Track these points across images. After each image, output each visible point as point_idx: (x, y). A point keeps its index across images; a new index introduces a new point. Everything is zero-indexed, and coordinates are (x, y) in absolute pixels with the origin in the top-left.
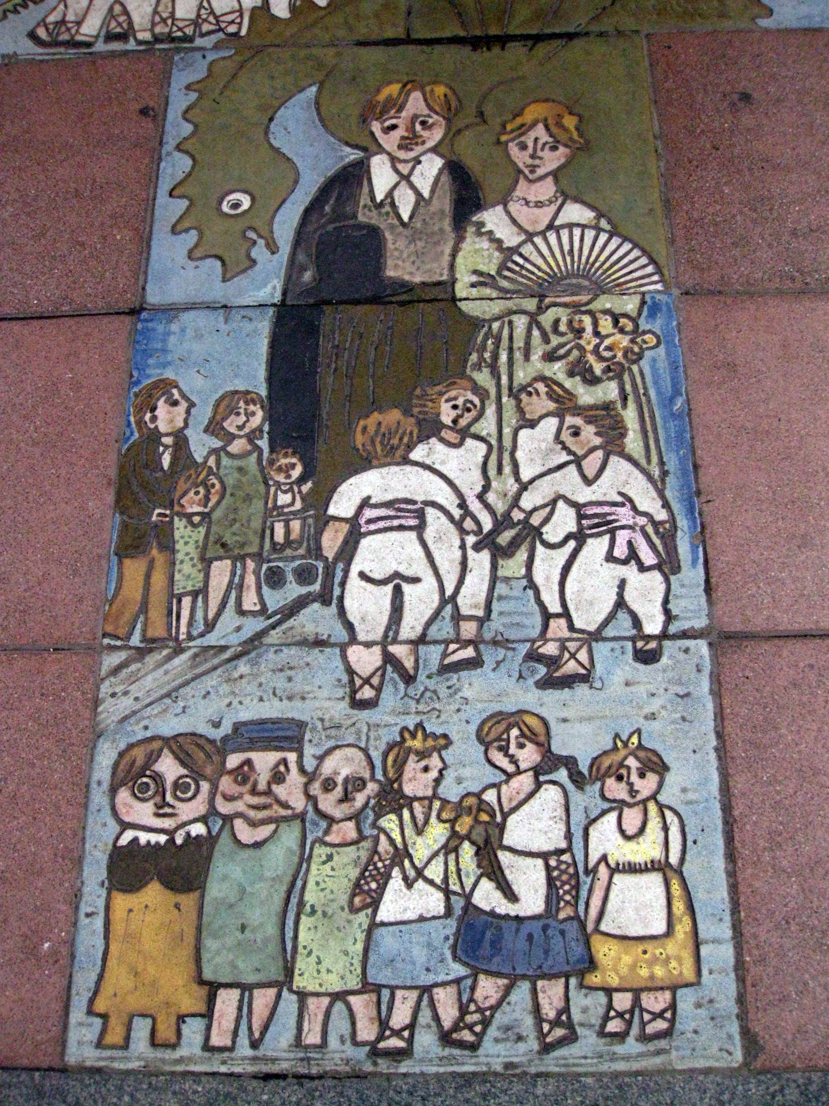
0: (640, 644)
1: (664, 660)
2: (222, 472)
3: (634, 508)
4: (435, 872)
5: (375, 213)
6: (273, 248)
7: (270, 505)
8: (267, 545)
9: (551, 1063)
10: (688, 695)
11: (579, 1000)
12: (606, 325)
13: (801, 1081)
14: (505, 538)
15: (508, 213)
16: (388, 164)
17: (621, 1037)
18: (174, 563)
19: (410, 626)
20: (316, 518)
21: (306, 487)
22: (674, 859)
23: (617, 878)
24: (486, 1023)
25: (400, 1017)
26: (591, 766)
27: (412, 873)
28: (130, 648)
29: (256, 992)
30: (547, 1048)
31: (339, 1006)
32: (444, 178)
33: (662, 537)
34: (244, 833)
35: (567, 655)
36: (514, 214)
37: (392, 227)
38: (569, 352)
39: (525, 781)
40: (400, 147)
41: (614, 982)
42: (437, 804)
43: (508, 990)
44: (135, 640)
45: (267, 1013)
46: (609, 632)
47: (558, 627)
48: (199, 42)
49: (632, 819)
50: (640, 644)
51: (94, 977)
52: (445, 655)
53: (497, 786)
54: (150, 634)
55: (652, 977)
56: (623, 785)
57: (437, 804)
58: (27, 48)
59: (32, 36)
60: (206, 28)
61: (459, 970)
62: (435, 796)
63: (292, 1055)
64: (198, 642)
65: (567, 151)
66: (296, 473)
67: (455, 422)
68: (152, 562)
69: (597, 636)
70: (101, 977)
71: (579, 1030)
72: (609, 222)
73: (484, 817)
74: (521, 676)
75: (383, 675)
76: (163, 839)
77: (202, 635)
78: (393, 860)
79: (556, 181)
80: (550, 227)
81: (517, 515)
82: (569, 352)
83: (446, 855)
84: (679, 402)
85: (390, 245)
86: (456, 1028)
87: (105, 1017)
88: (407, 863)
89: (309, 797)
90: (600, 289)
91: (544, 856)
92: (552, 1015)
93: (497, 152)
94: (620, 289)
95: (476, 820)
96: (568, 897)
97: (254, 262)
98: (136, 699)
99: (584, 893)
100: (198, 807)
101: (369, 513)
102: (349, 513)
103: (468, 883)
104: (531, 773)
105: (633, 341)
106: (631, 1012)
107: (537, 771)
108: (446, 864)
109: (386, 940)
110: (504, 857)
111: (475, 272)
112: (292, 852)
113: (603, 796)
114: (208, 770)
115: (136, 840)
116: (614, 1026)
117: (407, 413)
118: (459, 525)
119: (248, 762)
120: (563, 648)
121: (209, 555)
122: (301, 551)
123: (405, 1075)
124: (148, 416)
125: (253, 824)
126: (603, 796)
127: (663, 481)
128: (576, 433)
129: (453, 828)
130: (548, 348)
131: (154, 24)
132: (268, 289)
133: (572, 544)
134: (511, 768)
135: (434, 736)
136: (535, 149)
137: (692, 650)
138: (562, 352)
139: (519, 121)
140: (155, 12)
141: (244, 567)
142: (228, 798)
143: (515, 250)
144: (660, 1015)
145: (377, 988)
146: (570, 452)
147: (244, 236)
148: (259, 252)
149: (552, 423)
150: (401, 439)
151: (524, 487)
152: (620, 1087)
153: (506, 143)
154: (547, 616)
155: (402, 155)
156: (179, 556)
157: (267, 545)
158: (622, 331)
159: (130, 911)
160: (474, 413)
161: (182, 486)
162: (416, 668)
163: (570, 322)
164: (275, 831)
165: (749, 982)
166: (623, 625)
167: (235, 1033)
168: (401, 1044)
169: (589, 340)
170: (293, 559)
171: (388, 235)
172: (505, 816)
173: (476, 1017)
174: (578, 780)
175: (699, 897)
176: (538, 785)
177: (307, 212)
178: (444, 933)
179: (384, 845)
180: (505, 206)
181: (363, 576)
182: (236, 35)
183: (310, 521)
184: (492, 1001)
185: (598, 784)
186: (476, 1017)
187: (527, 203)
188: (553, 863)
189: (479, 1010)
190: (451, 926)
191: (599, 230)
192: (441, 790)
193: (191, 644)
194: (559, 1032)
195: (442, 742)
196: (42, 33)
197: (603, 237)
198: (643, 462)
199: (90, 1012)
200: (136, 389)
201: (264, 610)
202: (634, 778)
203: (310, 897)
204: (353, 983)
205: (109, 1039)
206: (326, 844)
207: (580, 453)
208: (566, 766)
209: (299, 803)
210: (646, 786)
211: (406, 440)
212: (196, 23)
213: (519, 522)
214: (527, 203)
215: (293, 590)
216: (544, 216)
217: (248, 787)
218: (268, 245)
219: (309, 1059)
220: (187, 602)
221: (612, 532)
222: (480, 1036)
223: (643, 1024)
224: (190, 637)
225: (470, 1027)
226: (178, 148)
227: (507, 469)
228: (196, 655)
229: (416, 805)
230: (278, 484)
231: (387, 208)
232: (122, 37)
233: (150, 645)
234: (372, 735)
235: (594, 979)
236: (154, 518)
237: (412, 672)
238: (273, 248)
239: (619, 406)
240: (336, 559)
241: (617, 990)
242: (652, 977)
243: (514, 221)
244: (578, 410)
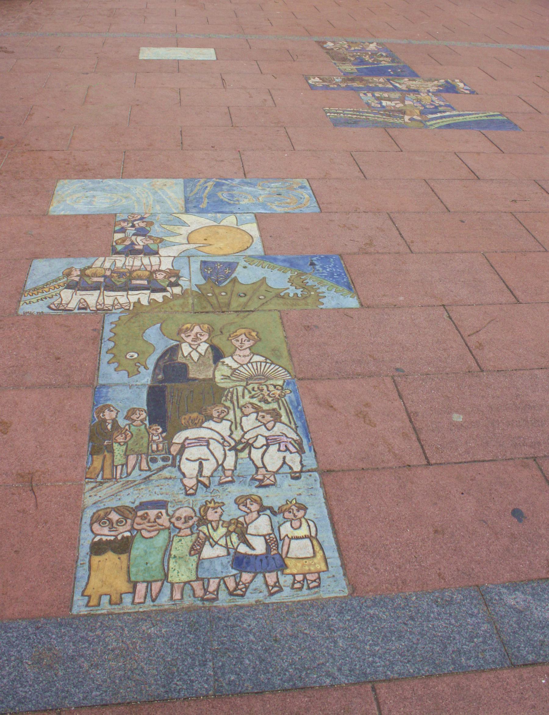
0: (293, 475)
1: (302, 478)
2: (131, 430)
3: (286, 436)
4: (222, 542)
5: (184, 359)
6: (146, 368)
7: (150, 440)
8: (150, 451)
9: (275, 599)
10: (312, 488)
11: (282, 579)
12: (271, 388)
13: (372, 598)
14: (240, 447)
15: (233, 359)
16: (188, 346)
17: (301, 589)
18: (113, 456)
19: (207, 472)
20: (168, 444)
21: (164, 434)
22: (313, 534)
23: (292, 541)
24: (247, 588)
25: (213, 587)
26: (279, 509)
27: (214, 543)
28: (97, 482)
29: (153, 584)
30: (271, 594)
31: (188, 587)
32: (210, 349)
33: (298, 444)
34: (144, 533)
35: (266, 479)
36: (236, 359)
37: (191, 363)
38: (259, 395)
39: (255, 515)
40: (192, 341)
41: (295, 571)
42: (221, 523)
43: (254, 577)
44: (99, 479)
45: (158, 590)
46: (281, 471)
47: (262, 471)
48: (114, 311)
49: (296, 524)
50: (293, 475)
51: (84, 584)
52: (220, 480)
53: (244, 516)
54: (105, 477)
55: (310, 570)
56: (291, 514)
57: (221, 523)
58: (47, 310)
59: (49, 307)
60: (116, 307)
61: (234, 572)
62: (220, 520)
63: (171, 603)
64: (124, 479)
65: (253, 342)
66: (160, 430)
67: (219, 416)
68: (105, 457)
69: (277, 472)
70: (87, 584)
71: (284, 588)
72: (270, 360)
73: (239, 525)
74: (249, 485)
75: (198, 486)
76: (112, 538)
77: (126, 477)
78: (205, 539)
79: (250, 349)
80: (249, 362)
81: (243, 440)
82: (259, 395)
83: (226, 537)
84: (300, 408)
85: (190, 368)
86: (235, 589)
87: (89, 597)
88: (211, 540)
89: (171, 522)
90: (268, 379)
91: (264, 536)
92: (272, 584)
93: (229, 342)
94: (276, 378)
95: (237, 526)
96: (274, 548)
97: (140, 372)
98: (100, 497)
99: (280, 545)
100: (128, 527)
101: (188, 441)
102: (181, 441)
103: (235, 545)
104: (256, 512)
105: (282, 392)
106: (303, 581)
107: (258, 512)
108: (226, 540)
109: (206, 564)
110: (248, 537)
111: (223, 375)
112: (166, 540)
113: (284, 518)
114: (130, 516)
115: (101, 539)
116: (297, 585)
117: (200, 413)
118: (222, 444)
119: (147, 513)
120: (264, 477)
121: (127, 454)
122: (164, 452)
123: (215, 607)
124: (101, 415)
125: (149, 531)
126: (284, 518)
127: (296, 429)
128: (263, 417)
129: (228, 529)
130: (251, 395)
131: (96, 306)
132: (146, 380)
133: (265, 447)
134: (248, 511)
135: (218, 503)
136: (242, 341)
137: (312, 475)
138: (256, 396)
139: (235, 334)
140: (97, 302)
141: (141, 457)
142: (138, 524)
143: (237, 369)
144: (315, 581)
145: (202, 579)
146: (261, 422)
147: (136, 365)
148: (142, 369)
149: (255, 415)
150: (199, 421)
151: (246, 433)
152: (302, 605)
153: (231, 340)
154: (257, 468)
155: (193, 343)
156: (116, 454)
157: (150, 451)
158: (277, 389)
159: (100, 561)
160: (225, 413)
161: (116, 434)
162: (210, 483)
163: (258, 388)
164: (158, 533)
165: (347, 569)
166: (286, 469)
167: (145, 598)
168: (214, 596)
169: (265, 392)
170: (160, 455)
171: (189, 365)
172: (248, 525)
173: (243, 586)
174: (274, 513)
175: (325, 545)
176: (259, 515)
177: (159, 360)
178: (227, 561)
179: (201, 535)
180: (232, 357)
181: (187, 459)
182: (128, 309)
183: (166, 444)
184: (249, 581)
185: (282, 514)
186: (243, 586)
187: (240, 356)
188: (267, 537)
189: (243, 584)
190: (230, 558)
191: (267, 363)
192: (222, 518)
193: (121, 480)
194: (276, 589)
195: (221, 504)
196: (53, 306)
197: (268, 365)
198: (288, 424)
199: (83, 595)
200: (96, 407)
201: (150, 469)
202: (295, 512)
203: (173, 553)
204: (194, 578)
205: (91, 603)
206: (179, 536)
207: (265, 422)
208: (269, 509)
209: (167, 524)
210: (300, 514)
211: (200, 421)
212: (113, 306)
213: (245, 442)
214: (240, 356)
215: (161, 463)
216: (248, 359)
217: (147, 520)
218: (145, 368)
219: (176, 604)
220: (119, 468)
221: (279, 444)
222: (245, 592)
223: (308, 585)
224: (121, 478)
225: (241, 589)
226: (109, 340)
227: (239, 428)
228: (123, 484)
229: (213, 523)
230: (153, 434)
231: (188, 358)
232: (85, 309)
233: (105, 480)
234: (194, 504)
235: (288, 571)
236: (105, 443)
237: (208, 485)
238: (146, 368)
239: (278, 410)
240: (177, 454)
241: (297, 574)
242: (310, 570)
243: (236, 361)
244: (263, 411)
